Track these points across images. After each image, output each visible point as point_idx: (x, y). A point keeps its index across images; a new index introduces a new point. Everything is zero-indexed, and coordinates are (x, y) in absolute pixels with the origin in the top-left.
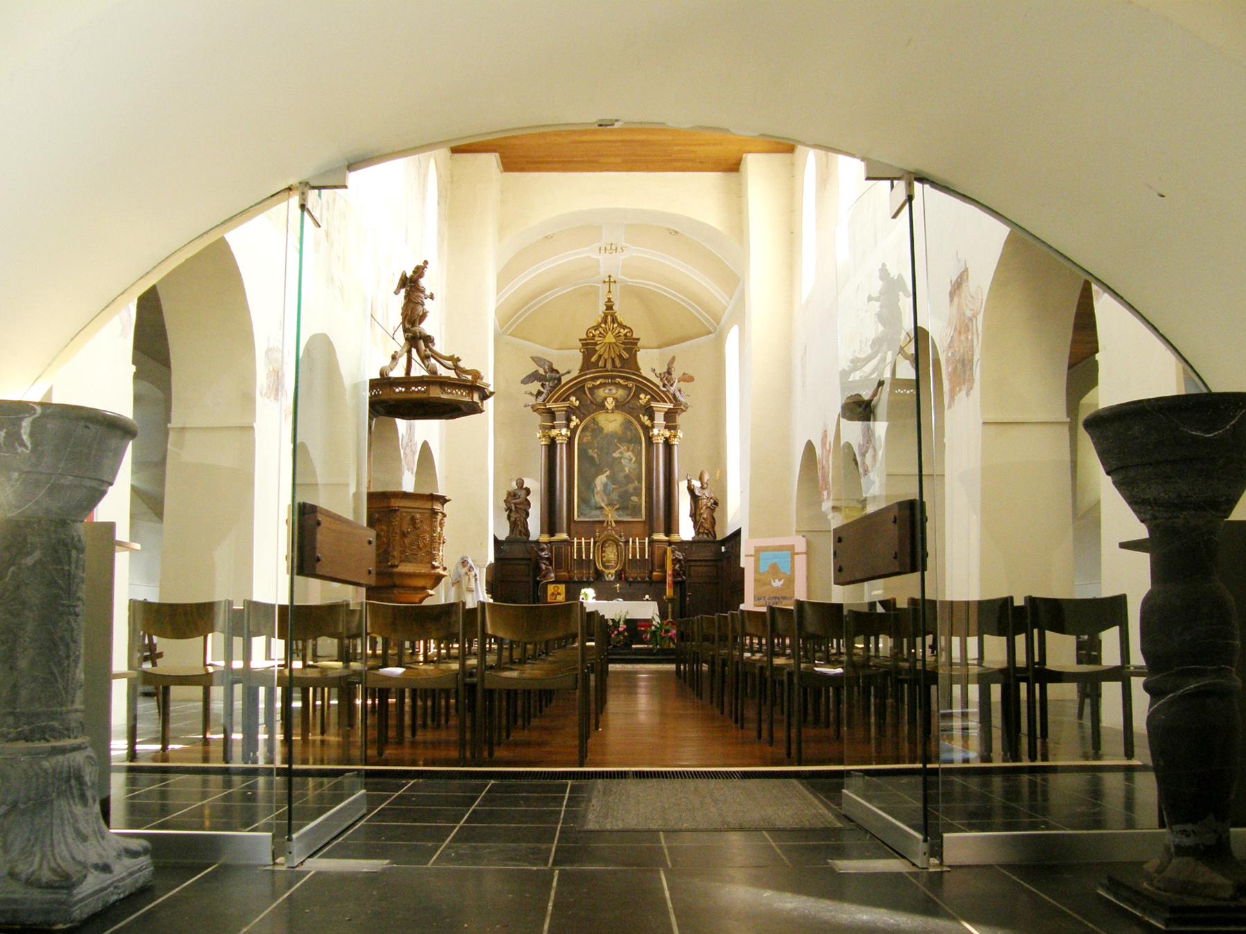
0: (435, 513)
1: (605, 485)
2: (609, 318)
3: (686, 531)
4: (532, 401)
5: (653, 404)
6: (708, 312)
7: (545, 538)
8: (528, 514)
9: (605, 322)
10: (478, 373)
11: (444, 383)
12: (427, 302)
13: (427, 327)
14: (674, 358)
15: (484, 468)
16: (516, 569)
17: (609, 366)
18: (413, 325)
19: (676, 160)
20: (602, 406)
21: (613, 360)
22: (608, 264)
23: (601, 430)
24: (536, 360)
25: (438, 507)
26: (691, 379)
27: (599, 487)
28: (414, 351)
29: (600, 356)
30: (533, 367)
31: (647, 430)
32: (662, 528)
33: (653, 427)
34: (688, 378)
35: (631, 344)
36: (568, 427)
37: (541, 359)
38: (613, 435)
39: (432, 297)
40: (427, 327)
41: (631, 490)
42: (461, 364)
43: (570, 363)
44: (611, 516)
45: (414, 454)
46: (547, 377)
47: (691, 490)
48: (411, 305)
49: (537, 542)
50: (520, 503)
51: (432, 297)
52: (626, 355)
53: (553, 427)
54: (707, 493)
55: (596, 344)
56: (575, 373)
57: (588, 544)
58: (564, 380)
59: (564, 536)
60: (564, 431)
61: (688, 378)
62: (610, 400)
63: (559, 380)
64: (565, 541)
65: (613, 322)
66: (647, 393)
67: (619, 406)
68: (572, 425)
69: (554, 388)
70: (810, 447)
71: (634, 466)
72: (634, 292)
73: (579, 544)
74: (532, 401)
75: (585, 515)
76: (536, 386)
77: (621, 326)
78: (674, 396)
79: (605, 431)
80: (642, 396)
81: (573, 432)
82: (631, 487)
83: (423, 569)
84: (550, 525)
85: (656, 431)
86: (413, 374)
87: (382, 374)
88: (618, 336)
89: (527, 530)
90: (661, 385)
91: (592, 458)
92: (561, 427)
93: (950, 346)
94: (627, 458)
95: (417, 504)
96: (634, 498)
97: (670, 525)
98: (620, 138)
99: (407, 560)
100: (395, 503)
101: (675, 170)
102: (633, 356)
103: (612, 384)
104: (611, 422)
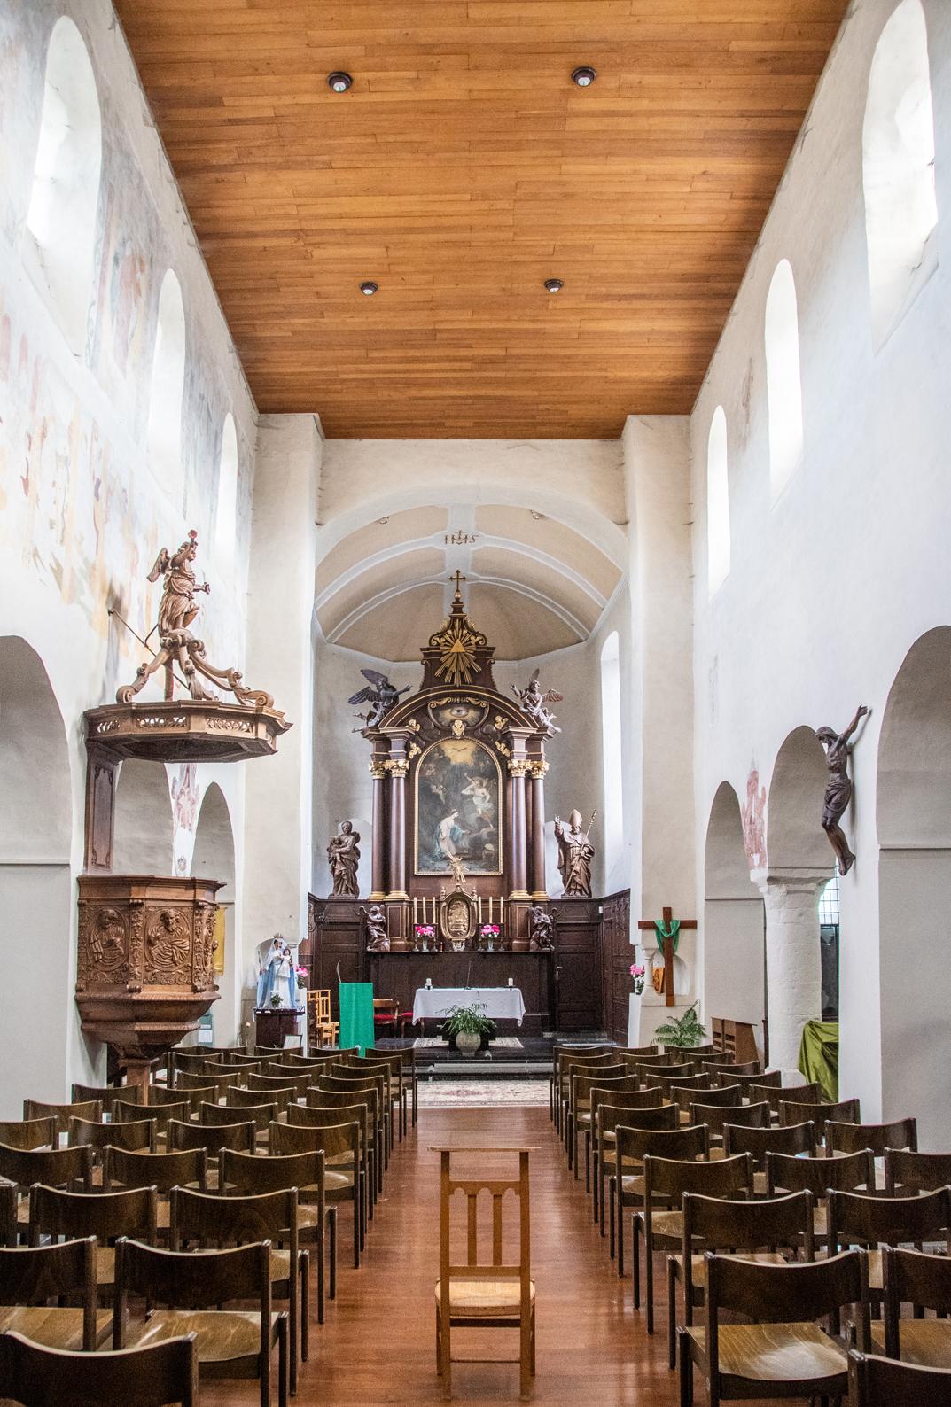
0: (197, 907)
1: (453, 830)
2: (457, 623)
3: (553, 885)
4: (363, 725)
5: (512, 729)
7: (378, 896)
8: (356, 866)
11: (211, 711)
16: (342, 946)
19: (543, 424)
20: (447, 732)
21: (462, 674)
22: (457, 557)
23: (449, 759)
24: (368, 674)
25: (203, 896)
28: (175, 663)
29: (446, 670)
30: (365, 683)
31: (504, 760)
32: (524, 884)
33: (511, 757)
35: (485, 655)
36: (407, 757)
37: (373, 673)
39: (206, 589)
40: (193, 631)
42: (243, 683)
43: (409, 677)
44: (461, 869)
48: (173, 597)
49: (367, 902)
50: (347, 853)
51: (206, 589)
52: (478, 668)
53: (388, 757)
55: (441, 655)
56: (415, 690)
58: (402, 698)
59: (402, 894)
60: (402, 762)
62: (458, 723)
63: (396, 698)
64: (403, 901)
65: (462, 628)
66: (504, 716)
67: (470, 732)
68: (411, 755)
69: (393, 705)
70: (726, 796)
71: (490, 806)
73: (420, 903)
74: (363, 725)
76: (367, 706)
77: (472, 632)
78: (538, 718)
79: (453, 763)
80: (498, 719)
81: (413, 762)
82: (485, 832)
84: (385, 884)
85: (515, 763)
87: (119, 699)
88: (468, 644)
89: (354, 884)
91: (437, 796)
92: (398, 756)
94: (479, 797)
95: (174, 893)
96: (489, 847)
99: (153, 981)
100: (137, 894)
103: (461, 704)
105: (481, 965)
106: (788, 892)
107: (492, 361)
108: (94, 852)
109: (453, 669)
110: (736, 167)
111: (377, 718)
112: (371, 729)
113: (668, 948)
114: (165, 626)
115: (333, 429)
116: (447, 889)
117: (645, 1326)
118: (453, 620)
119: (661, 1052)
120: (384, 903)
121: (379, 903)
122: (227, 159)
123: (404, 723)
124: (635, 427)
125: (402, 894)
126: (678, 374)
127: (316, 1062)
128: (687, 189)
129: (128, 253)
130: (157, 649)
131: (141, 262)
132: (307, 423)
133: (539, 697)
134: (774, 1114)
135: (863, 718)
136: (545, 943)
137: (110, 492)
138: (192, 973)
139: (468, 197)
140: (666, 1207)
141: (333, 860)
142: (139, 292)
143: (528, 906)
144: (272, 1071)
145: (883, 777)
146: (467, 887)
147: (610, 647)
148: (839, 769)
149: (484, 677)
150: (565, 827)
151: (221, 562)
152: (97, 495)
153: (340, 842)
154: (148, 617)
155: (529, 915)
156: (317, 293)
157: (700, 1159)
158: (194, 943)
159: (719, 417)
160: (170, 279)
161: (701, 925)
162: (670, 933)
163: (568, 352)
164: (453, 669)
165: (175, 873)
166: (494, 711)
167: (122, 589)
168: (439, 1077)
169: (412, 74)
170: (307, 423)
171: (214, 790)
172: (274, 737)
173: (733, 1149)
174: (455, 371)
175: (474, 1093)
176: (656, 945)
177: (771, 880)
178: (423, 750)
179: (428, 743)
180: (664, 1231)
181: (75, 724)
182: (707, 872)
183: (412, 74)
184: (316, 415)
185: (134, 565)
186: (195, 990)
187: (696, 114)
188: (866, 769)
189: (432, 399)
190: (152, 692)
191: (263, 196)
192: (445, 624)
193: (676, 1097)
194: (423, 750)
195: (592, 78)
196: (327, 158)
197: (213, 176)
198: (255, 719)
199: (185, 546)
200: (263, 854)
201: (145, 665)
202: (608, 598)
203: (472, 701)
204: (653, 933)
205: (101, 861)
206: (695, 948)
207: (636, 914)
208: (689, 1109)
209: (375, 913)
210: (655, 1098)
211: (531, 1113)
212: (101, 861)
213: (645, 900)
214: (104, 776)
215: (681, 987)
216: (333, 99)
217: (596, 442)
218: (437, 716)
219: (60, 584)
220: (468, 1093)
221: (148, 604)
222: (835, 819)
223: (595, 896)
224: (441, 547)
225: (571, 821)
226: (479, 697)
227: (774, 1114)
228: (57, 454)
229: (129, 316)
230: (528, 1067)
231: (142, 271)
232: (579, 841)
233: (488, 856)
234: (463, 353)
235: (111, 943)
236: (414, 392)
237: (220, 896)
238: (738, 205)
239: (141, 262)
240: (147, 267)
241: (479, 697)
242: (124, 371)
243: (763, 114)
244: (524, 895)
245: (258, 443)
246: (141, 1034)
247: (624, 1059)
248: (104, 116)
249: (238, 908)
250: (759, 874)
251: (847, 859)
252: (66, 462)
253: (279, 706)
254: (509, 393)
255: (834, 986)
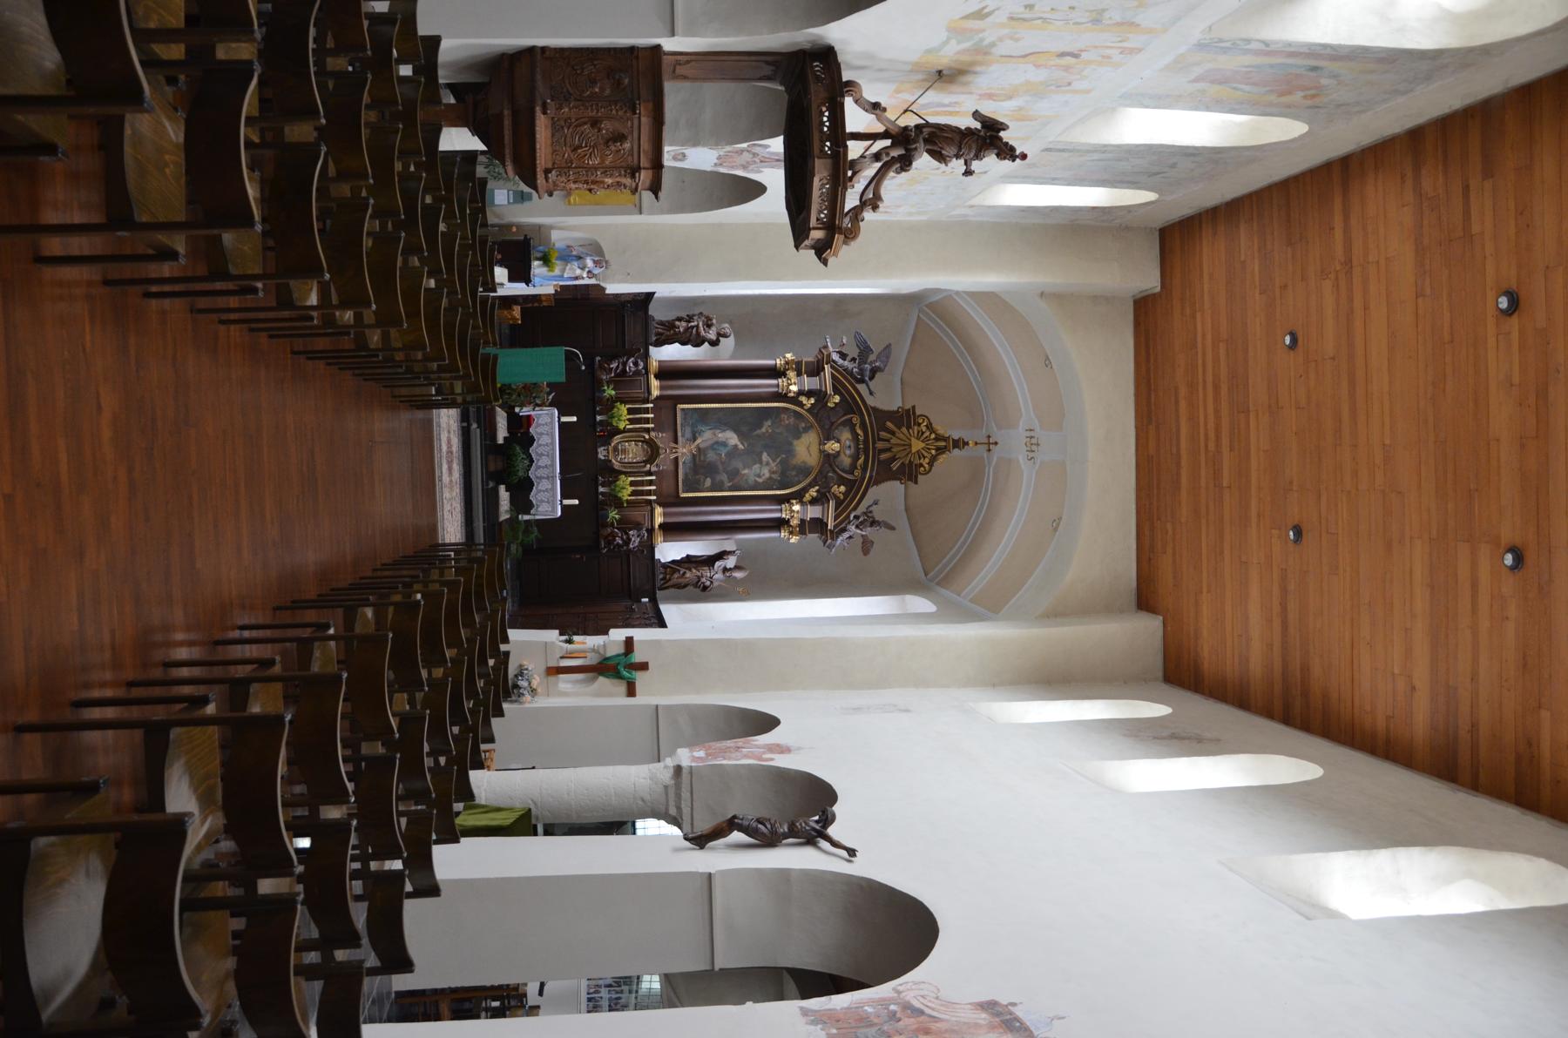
0: (634, 171)
1: (724, 444)
3: (669, 551)
5: (832, 504)
6: (954, 567)
7: (654, 365)
8: (683, 344)
9: (937, 439)
10: (854, 238)
12: (958, 165)
13: (923, 161)
14: (893, 528)
15: (733, 274)
16: (602, 331)
17: (880, 445)
18: (926, 141)
21: (889, 450)
22: (1013, 443)
23: (798, 438)
25: (645, 177)
26: (866, 551)
27: (721, 436)
28: (888, 142)
29: (893, 433)
30: (877, 348)
31: (798, 496)
33: (802, 503)
34: (867, 546)
35: (909, 473)
36: (800, 393)
38: (790, 452)
39: (968, 173)
40: (923, 161)
41: (718, 478)
42: (868, 215)
43: (884, 395)
44: (684, 451)
45: (744, 167)
46: (867, 363)
47: (721, 555)
48: (957, 138)
49: (646, 356)
50: (698, 333)
51: (968, 173)
52: (895, 466)
53: (799, 374)
54: (719, 576)
55: (909, 428)
56: (871, 401)
57: (647, 421)
58: (862, 388)
59: (655, 393)
60: (794, 388)
61: (867, 546)
63: (862, 381)
64: (649, 392)
65: (938, 449)
66: (846, 494)
67: (829, 459)
68: (803, 399)
70: (767, 723)
72: (976, 475)
73: (646, 411)
75: (684, 419)
76: (853, 352)
77: (933, 459)
78: (844, 530)
83: (543, 156)
84: (669, 373)
85: (797, 508)
86: (850, 143)
87: (850, 83)
88: (920, 455)
90: (858, 512)
91: (760, 427)
92: (801, 383)
93: (907, 1007)
94: (763, 469)
95: (646, 145)
96: (708, 482)
97: (674, 530)
98: (1184, 453)
99: (555, 127)
101: (1138, 526)
102: (894, 476)
103: (857, 449)
104: (807, 449)
105: (584, 467)
106: (666, 787)
107: (1217, 474)
108: (688, 62)
109: (894, 441)
110: (1420, 721)
111: (840, 361)
112: (829, 355)
113: (605, 668)
114: (926, 130)
115: (1144, 308)
116: (661, 438)
117: (219, 636)
118: (945, 439)
119: (503, 647)
120: (647, 373)
121: (646, 368)
122: (1426, 184)
123: (836, 391)
124: (1149, 628)
125: (655, 393)
126: (1206, 665)
127: (474, 302)
128: (1396, 671)
129: (1324, 81)
130: (902, 123)
131: (1314, 96)
132: (1150, 281)
133: (868, 531)
134: (442, 760)
135: (844, 853)
136: (609, 543)
137: (1067, 68)
138: (564, 168)
139: (1387, 442)
140: (342, 657)
141: (690, 319)
142: (1282, 94)
143: (647, 524)
144: (463, 256)
145: (784, 875)
146: (663, 462)
147: (919, 604)
148: (793, 832)
149: (886, 473)
150: (731, 562)
151: (1009, 191)
152: (1063, 55)
153: (709, 326)
154: (937, 114)
155: (638, 526)
156: (1286, 286)
157: (388, 675)
158: (596, 169)
159: (1159, 710)
160: (1297, 128)
161: (631, 701)
162: (620, 669)
163: (1227, 552)
164: (894, 441)
165: (668, 150)
166: (850, 485)
167: (966, 84)
168: (466, 435)
169: (1516, 380)
170: (1150, 281)
171: (757, 189)
172: (812, 247)
173: (404, 719)
174: (1206, 435)
175: (450, 469)
176: (609, 654)
177: (678, 770)
178: (808, 410)
179: (815, 416)
180: (317, 653)
181: (821, 37)
182: (687, 707)
183: (1516, 380)
184: (1158, 289)
185: (990, 96)
186: (547, 171)
187: (1474, 678)
188: (792, 858)
189: (1177, 411)
190: (856, 119)
191: (1388, 222)
192: (941, 431)
193: (456, 662)
194: (808, 410)
195: (1513, 568)
196: (1428, 291)
197: (1409, 174)
198: (831, 227)
199: (1012, 149)
200: (698, 244)
201: (885, 110)
202: (971, 601)
203: (861, 461)
204: (621, 650)
205: (679, 70)
206: (606, 696)
207: (640, 634)
208: (446, 675)
209: (636, 364)
210: (455, 642)
211: (433, 529)
212: (679, 70)
213: (657, 643)
214: (767, 70)
215: (565, 682)
216: (1490, 295)
217: (1134, 584)
218: (844, 424)
219: (967, 17)
220: (450, 463)
221: (951, 114)
222: (741, 829)
223: (659, 594)
224: (1022, 425)
225: (737, 568)
226: (864, 469)
227: (442, 760)
228: (1104, 10)
229: (1255, 84)
230: (479, 525)
231: (1305, 97)
232: (716, 574)
233: (698, 482)
234: (1225, 441)
235: (593, 82)
236: (1183, 391)
237: (647, 196)
238: (1381, 724)
239: (1314, 96)
240: (1309, 102)
241: (864, 469)
242: (1196, 80)
243: (1474, 747)
244: (659, 520)
245: (1128, 228)
246: (500, 117)
247: (495, 612)
248: (1470, 51)
249: (636, 219)
250: (684, 757)
251: (700, 841)
252: (1096, 21)
253: (845, 253)
254: (1184, 493)
255: (568, 828)
